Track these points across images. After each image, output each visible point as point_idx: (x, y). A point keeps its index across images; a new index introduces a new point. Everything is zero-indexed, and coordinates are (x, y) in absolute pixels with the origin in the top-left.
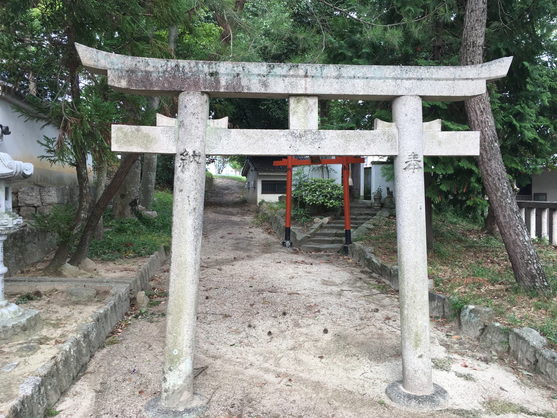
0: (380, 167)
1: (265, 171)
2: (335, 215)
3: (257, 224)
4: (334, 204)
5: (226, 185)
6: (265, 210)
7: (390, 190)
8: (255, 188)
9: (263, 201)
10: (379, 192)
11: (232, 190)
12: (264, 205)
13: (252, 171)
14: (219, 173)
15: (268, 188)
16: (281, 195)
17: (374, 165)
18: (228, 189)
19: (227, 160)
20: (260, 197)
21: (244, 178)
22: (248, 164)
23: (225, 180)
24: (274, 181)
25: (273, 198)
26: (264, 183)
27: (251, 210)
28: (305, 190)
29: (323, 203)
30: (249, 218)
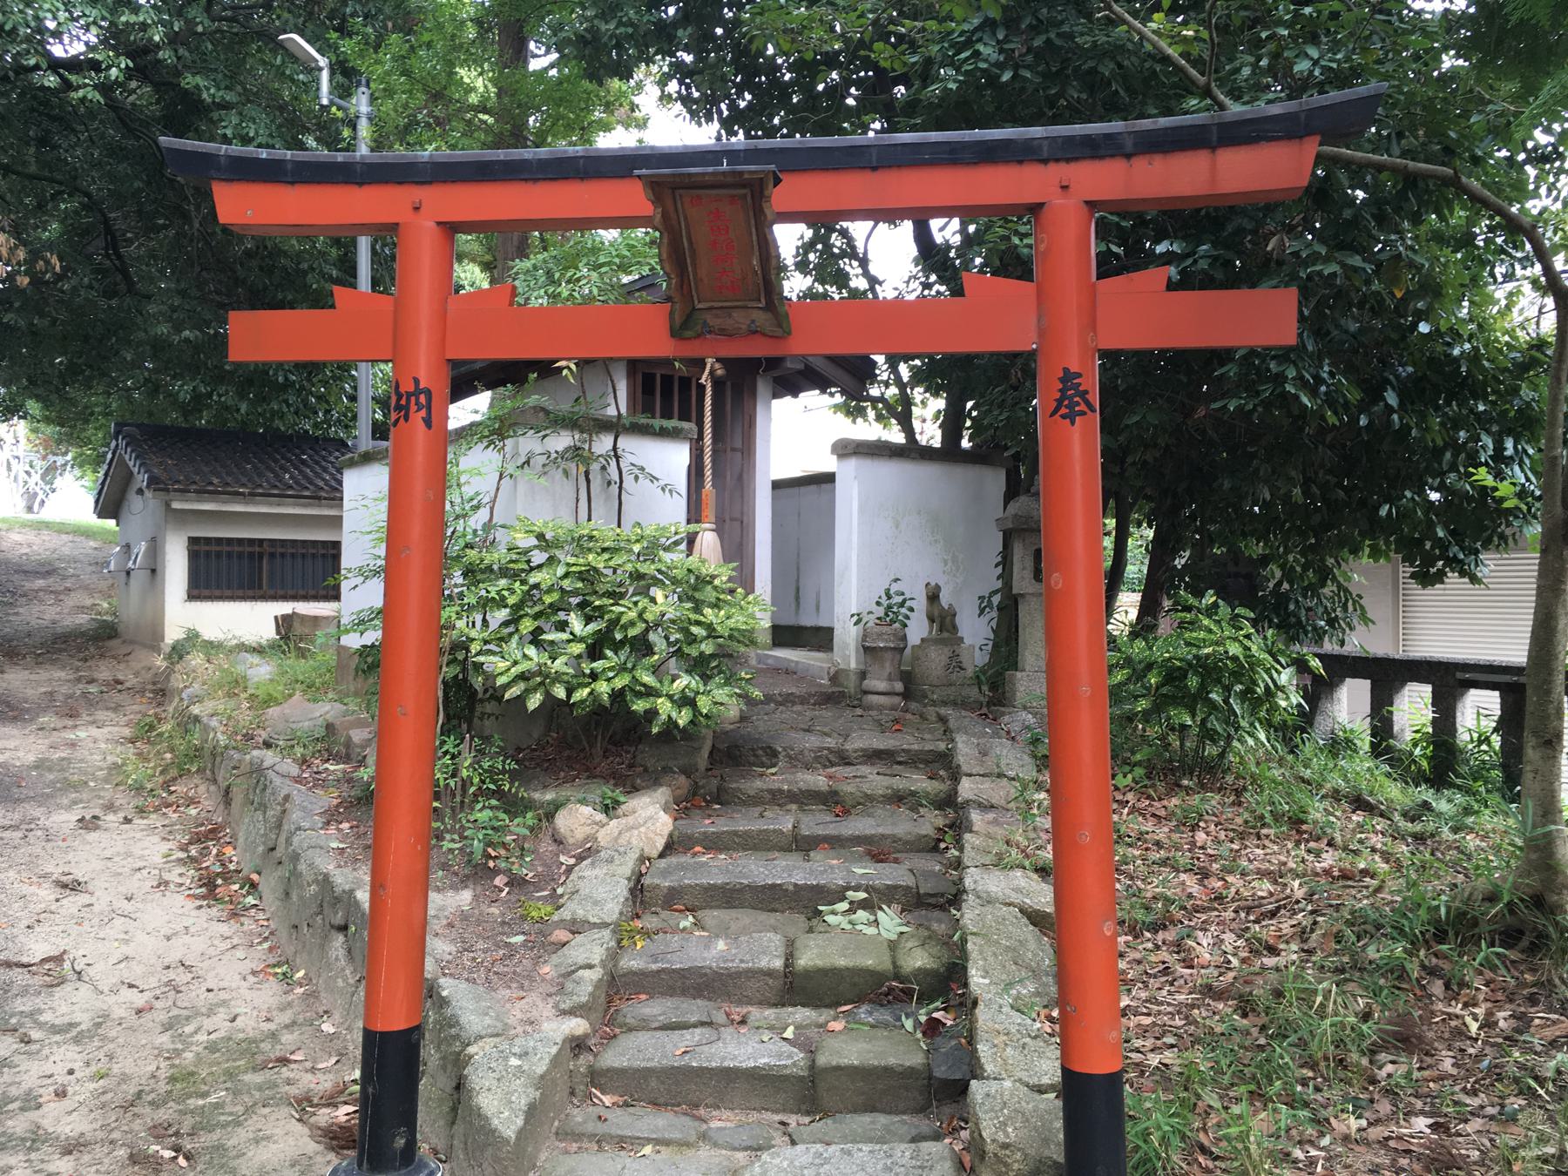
0: (889, 471)
1: (203, 493)
2: (687, 772)
3: (138, 789)
4: (704, 704)
5: (45, 555)
6: (198, 699)
7: (945, 599)
8: (154, 571)
9: (192, 637)
10: (892, 612)
11: (64, 578)
12: (196, 660)
13: (140, 492)
14: (30, 509)
15: (223, 571)
16: (285, 608)
17: (852, 464)
18: (49, 573)
19: (60, 460)
20: (182, 614)
21: (110, 524)
22: (122, 462)
23: (46, 535)
24: (251, 541)
25: (254, 620)
26: (200, 552)
27: (132, 681)
28: (486, 604)
29: (618, 695)
30: (99, 741)
